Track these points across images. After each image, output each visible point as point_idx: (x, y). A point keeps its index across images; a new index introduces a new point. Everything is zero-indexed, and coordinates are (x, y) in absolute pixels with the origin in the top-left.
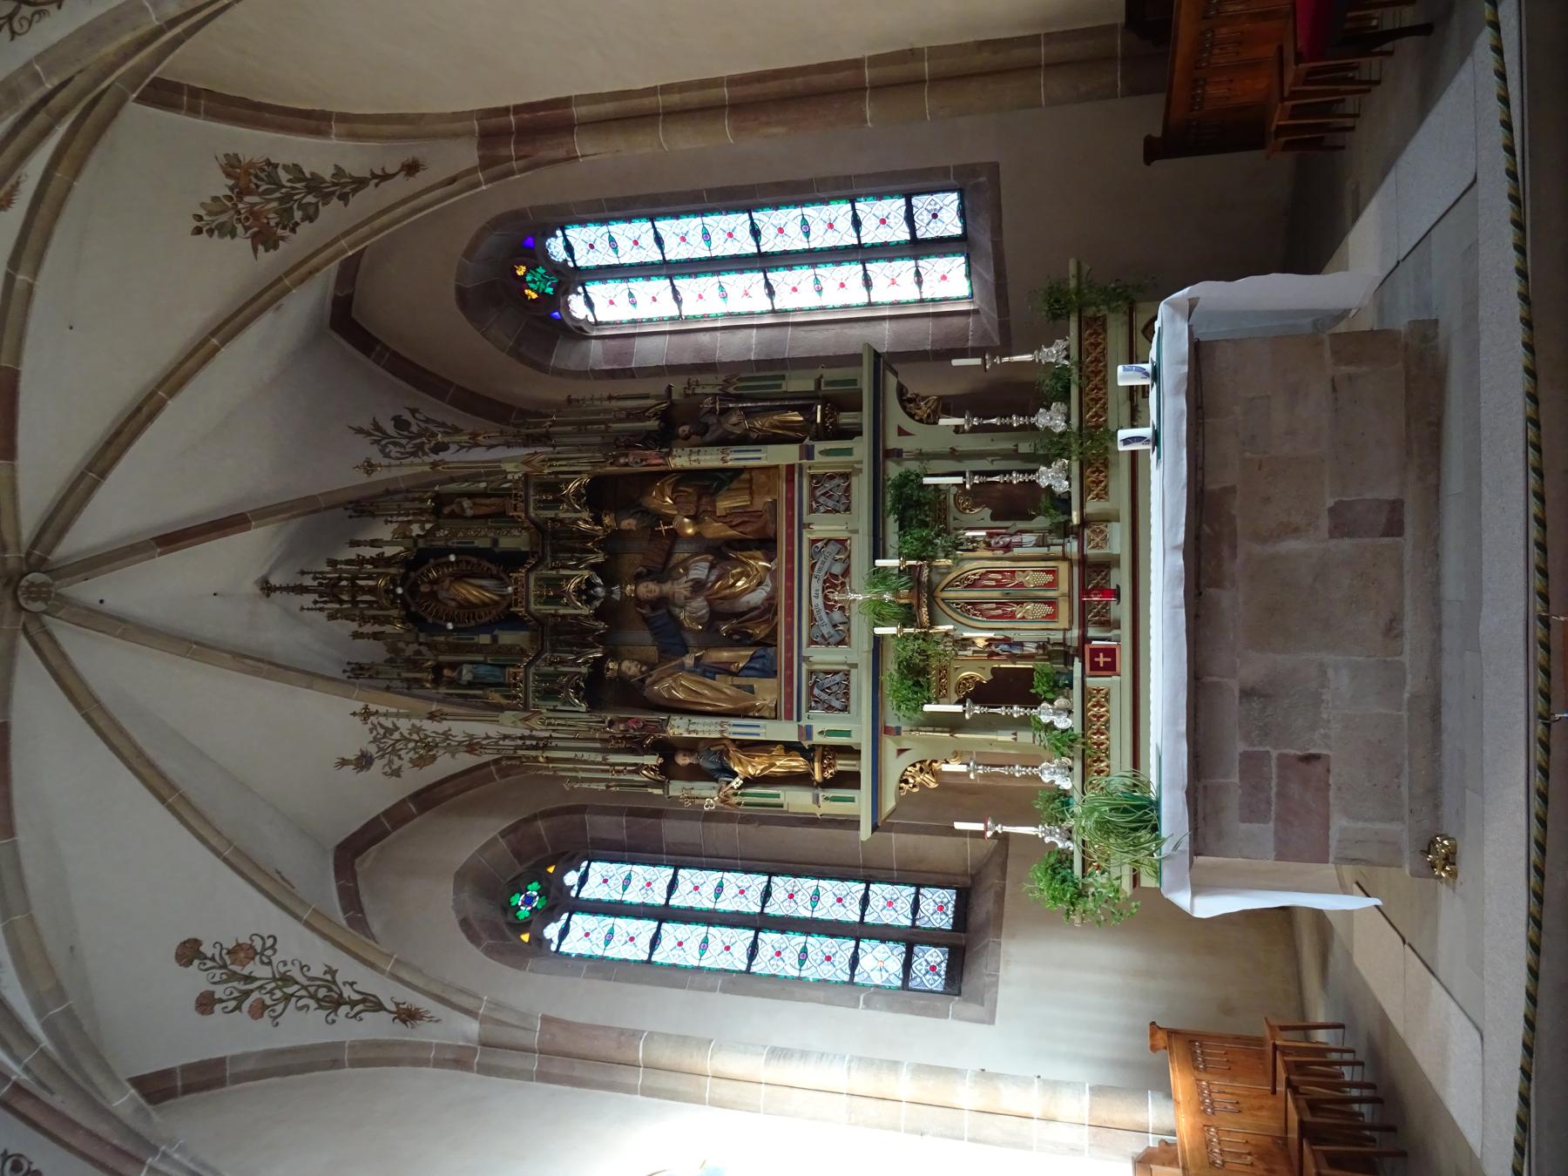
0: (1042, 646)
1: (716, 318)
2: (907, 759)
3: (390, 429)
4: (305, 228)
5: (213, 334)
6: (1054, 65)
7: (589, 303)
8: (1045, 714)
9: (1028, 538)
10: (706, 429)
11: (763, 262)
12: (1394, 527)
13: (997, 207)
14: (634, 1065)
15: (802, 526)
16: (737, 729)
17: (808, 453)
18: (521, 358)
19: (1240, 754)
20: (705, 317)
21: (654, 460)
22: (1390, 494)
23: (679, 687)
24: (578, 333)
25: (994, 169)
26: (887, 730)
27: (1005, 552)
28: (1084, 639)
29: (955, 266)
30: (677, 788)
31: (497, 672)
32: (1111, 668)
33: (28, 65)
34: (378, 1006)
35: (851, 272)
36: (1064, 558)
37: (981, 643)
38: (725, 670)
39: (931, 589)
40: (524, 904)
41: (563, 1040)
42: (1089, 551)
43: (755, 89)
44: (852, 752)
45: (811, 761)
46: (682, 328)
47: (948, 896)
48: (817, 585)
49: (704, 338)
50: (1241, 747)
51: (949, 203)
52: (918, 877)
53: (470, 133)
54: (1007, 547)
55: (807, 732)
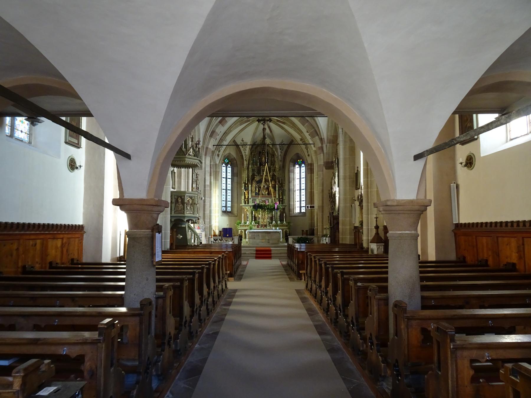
0: (259, 221)
1: (295, 183)
2: (248, 208)
5: (291, 135)
6: (312, 222)
7: (298, 168)
8: (253, 222)
9: (269, 220)
10: (280, 188)
11: (300, 190)
12: (268, 243)
16: (250, 192)
17: (277, 199)
18: (291, 160)
20: (295, 182)
21: (277, 183)
23: (254, 185)
24: (294, 166)
25: (305, 216)
26: (250, 207)
27: (277, 121)
28: (260, 225)
29: (299, 211)
30: (243, 184)
32: (257, 227)
33: (308, 140)
34: (219, 152)
35: (299, 200)
36: (267, 223)
37: (259, 216)
38: (256, 190)
39: (264, 212)
41: (217, 173)
42: (267, 225)
44: (248, 203)
46: (294, 179)
47: (230, 210)
48: (264, 200)
51: (304, 211)
52: (232, 207)
54: (268, 218)
55: (250, 199)
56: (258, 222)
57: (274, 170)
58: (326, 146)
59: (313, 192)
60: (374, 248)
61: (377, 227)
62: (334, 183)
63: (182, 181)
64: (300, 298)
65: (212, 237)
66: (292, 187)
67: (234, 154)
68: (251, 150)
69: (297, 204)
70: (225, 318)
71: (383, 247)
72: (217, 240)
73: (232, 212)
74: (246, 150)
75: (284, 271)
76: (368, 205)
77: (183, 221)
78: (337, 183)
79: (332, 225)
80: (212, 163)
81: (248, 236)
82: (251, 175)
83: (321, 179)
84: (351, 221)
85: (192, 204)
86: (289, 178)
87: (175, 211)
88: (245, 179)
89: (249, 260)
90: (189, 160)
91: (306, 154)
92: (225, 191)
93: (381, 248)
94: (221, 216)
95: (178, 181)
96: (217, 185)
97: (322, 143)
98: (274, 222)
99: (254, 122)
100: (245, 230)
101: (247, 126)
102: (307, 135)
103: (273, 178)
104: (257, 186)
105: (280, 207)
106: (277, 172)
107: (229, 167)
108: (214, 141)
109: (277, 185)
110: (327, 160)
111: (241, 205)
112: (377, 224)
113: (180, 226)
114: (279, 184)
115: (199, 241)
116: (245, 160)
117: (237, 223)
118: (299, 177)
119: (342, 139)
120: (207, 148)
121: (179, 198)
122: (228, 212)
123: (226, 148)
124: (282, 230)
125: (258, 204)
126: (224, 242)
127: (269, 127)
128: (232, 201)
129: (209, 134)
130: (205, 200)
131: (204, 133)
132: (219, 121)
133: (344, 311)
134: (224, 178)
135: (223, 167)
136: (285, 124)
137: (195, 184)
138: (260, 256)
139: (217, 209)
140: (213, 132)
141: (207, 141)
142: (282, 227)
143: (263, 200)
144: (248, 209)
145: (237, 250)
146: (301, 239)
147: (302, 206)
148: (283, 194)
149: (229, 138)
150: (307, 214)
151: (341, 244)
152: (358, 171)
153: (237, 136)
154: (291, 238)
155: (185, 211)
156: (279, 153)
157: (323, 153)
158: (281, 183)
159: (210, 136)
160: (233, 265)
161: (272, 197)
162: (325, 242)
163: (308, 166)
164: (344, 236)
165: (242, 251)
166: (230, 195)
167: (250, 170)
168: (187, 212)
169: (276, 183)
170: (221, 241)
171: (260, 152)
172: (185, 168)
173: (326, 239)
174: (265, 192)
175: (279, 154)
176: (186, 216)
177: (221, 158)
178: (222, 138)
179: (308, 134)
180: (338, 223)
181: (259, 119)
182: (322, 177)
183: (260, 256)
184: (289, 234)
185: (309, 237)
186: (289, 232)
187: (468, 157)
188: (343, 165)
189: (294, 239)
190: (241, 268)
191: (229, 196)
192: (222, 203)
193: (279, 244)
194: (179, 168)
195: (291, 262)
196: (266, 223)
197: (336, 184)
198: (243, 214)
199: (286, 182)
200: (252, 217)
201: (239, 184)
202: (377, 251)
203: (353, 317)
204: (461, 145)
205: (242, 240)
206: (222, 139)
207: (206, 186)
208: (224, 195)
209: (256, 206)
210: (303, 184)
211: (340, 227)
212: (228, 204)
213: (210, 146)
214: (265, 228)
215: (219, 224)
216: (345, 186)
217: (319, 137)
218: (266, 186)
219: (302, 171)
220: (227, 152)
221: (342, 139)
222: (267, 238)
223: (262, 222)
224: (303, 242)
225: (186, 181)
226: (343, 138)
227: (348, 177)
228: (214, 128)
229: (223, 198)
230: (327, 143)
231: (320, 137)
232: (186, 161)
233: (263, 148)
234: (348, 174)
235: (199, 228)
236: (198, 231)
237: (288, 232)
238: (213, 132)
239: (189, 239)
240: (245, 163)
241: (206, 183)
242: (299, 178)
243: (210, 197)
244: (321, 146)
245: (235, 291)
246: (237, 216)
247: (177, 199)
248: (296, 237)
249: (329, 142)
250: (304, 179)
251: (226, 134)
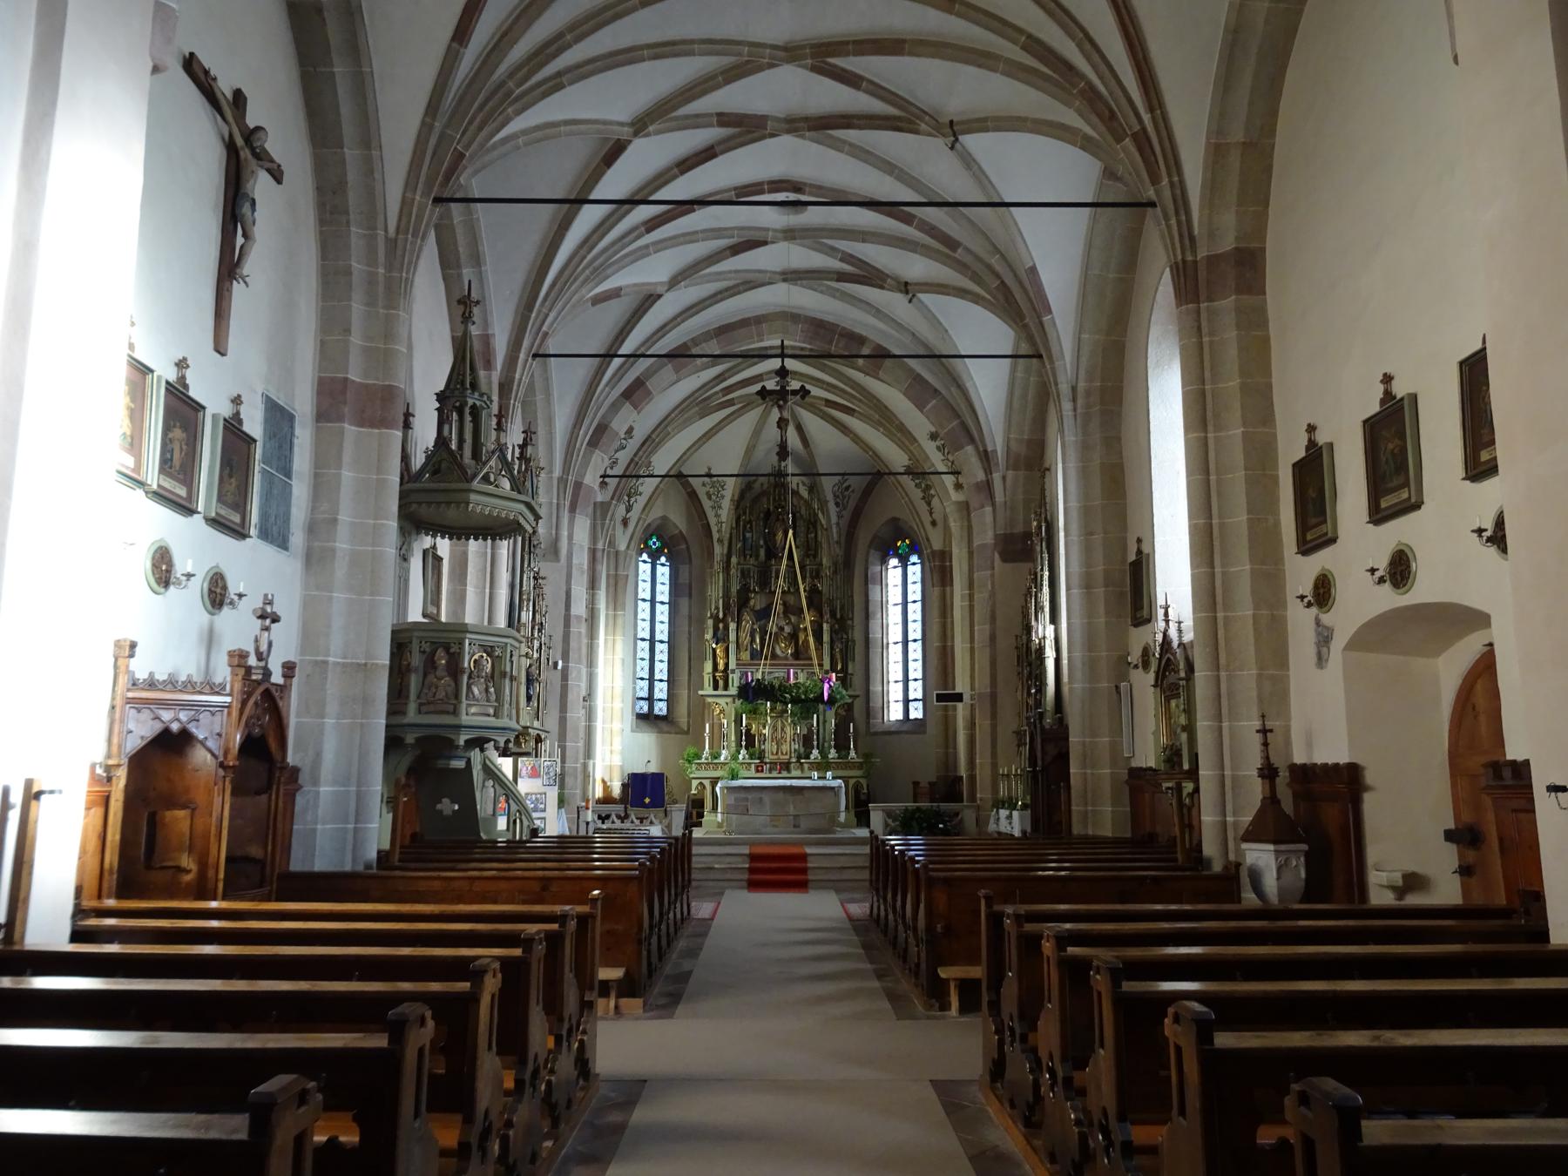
0: (764, 751)
2: (725, 706)
3: (844, 485)
4: (912, 484)
5: (874, 452)
6: (947, 754)
7: (895, 567)
8: (743, 751)
9: (797, 746)
11: (905, 642)
12: (795, 826)
15: (802, 670)
16: (732, 647)
19: (1131, 564)
20: (887, 615)
21: (827, 616)
24: (884, 561)
25: (925, 732)
28: (766, 763)
29: (900, 716)
30: (710, 622)
31: (749, 547)
32: (757, 771)
34: (628, 511)
38: (753, 640)
39: (781, 716)
40: (654, 543)
41: (620, 584)
44: (726, 687)
46: (883, 606)
47: (664, 712)
49: (879, 615)
50: (750, 797)
52: (671, 700)
55: (733, 671)
56: (760, 753)
57: (817, 575)
58: (1004, 478)
59: (949, 649)
60: (1261, 863)
61: (1268, 772)
63: (468, 592)
64: (971, 1159)
66: (875, 633)
67: (679, 520)
68: (737, 508)
69: (895, 692)
70: (630, 1124)
71: (1302, 859)
72: (608, 817)
74: (720, 507)
77: (450, 745)
78: (1047, 609)
79: (1039, 763)
80: (600, 546)
81: (723, 801)
82: (738, 592)
83: (986, 595)
84: (1115, 748)
85: (492, 677)
86: (867, 602)
88: (717, 602)
89: (722, 894)
90: (483, 502)
91: (927, 519)
92: (646, 645)
95: (452, 593)
96: (620, 621)
97: (988, 470)
98: (815, 752)
99: (750, 407)
100: (714, 781)
102: (930, 448)
104: (755, 627)
105: (839, 693)
106: (825, 579)
107: (663, 565)
108: (603, 460)
109: (825, 626)
110: (1006, 529)
111: (700, 692)
113: (441, 763)
115: (526, 823)
118: (899, 600)
119: (1073, 439)
120: (578, 485)
122: (658, 717)
125: (758, 680)
126: (632, 826)
127: (800, 429)
128: (671, 681)
131: (568, 436)
132: (623, 388)
133: (1024, 1038)
134: (644, 600)
135: (641, 564)
136: (852, 416)
137: (528, 610)
138: (766, 865)
140: (602, 429)
141: (577, 461)
142: (842, 769)
143: (777, 675)
144: (724, 706)
145: (678, 852)
146: (917, 816)
147: (910, 698)
148: (847, 655)
150: (933, 729)
152: (1139, 552)
153: (688, 458)
154: (881, 813)
155: (460, 702)
156: (832, 518)
158: (838, 616)
160: (640, 942)
161: (812, 665)
162: (1004, 827)
167: (733, 571)
169: (821, 616)
170: (623, 822)
171: (768, 514)
172: (485, 539)
173: (1010, 817)
174: (784, 649)
175: (834, 519)
176: (464, 723)
178: (636, 459)
180: (1063, 757)
183: (766, 865)
185: (944, 806)
186: (868, 786)
189: (889, 814)
191: (661, 661)
192: (638, 688)
193: (834, 832)
194: (459, 539)
197: (1043, 611)
198: (707, 725)
199: (855, 614)
201: (697, 622)
202: (1278, 878)
203: (1109, 1111)
204: (1468, 482)
205: (703, 817)
207: (573, 622)
208: (643, 659)
209: (751, 691)
212: (656, 690)
213: (591, 479)
214: (785, 774)
215: (623, 759)
216: (1090, 613)
217: (977, 448)
218: (787, 629)
220: (656, 513)
221: (1073, 439)
222: (791, 810)
223: (772, 754)
224: (925, 825)
226: (1076, 435)
229: (638, 668)
230: (1007, 469)
231: (981, 449)
235: (535, 774)
236: (525, 786)
237: (865, 786)
238: (602, 429)
240: (719, 550)
241: (572, 610)
243: (591, 663)
245: (633, 1090)
246: (687, 733)
247: (433, 653)
249: (1014, 462)
251: (652, 442)
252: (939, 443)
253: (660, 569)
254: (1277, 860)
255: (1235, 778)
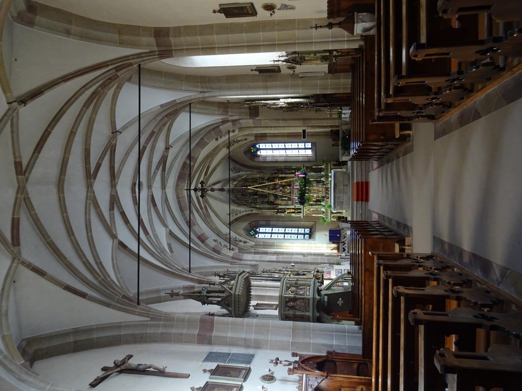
0: (322, 196)
1: (278, 155)
5: (222, 159)
6: (323, 135)
7: (260, 152)
8: (322, 203)
9: (320, 185)
10: (282, 172)
11: (286, 149)
12: (347, 186)
13: (316, 146)
14: (274, 246)
15: (295, 183)
16: (287, 207)
18: (251, 160)
21: (277, 175)
22: (347, 184)
23: (280, 202)
24: (258, 156)
28: (326, 196)
29: (310, 151)
30: (279, 214)
32: (328, 198)
34: (241, 241)
35: (297, 151)
37: (315, 196)
38: (285, 200)
39: (310, 190)
40: (252, 233)
41: (266, 244)
43: (289, 134)
44: (300, 209)
45: (295, 210)
46: (273, 157)
47: (309, 229)
49: (276, 158)
52: (304, 227)
53: (254, 136)
56: (322, 198)
57: (263, 179)
58: (231, 116)
59: (288, 134)
61: (330, 26)
62: (275, 105)
65: (341, 255)
66: (282, 159)
68: (241, 205)
69: (302, 152)
71: (360, 14)
72: (344, 248)
73: (311, 228)
74: (240, 211)
75: (390, 164)
76: (298, 43)
77: (319, 301)
78: (275, 101)
82: (268, 205)
83: (270, 122)
84: (322, 78)
87: (306, 311)
91: (244, 142)
92: (286, 235)
93: (362, 16)
94: (315, 240)
96: (278, 244)
97: (228, 121)
98: (322, 179)
100: (332, 213)
101: (213, 210)
102: (220, 141)
103: (270, 180)
104: (280, 199)
106: (264, 176)
107: (259, 230)
111: (302, 217)
112: (325, 26)
113: (326, 304)
114: (278, 173)
116: (251, 211)
117: (323, 222)
120: (233, 258)
121: (288, 305)
122: (310, 232)
123: (237, 233)
124: (331, 169)
125: (298, 198)
126: (347, 240)
128: (298, 227)
129: (216, 255)
130: (294, 262)
134: (271, 236)
135: (259, 237)
137: (274, 275)
138: (360, 196)
139: (306, 245)
140: (215, 250)
141: (225, 258)
142: (328, 170)
143: (296, 192)
144: (307, 210)
146: (344, 145)
148: (290, 169)
149: (225, 230)
150: (314, 140)
151: (351, 90)
152: (256, 70)
155: (305, 298)
156: (244, 174)
157: (239, 119)
158: (277, 171)
159: (219, 255)
160: (386, 238)
161: (293, 180)
162: (348, 116)
163: (258, 140)
164: (342, 87)
165: (358, 220)
166: (290, 229)
167: (262, 207)
168: (306, 295)
169: (277, 177)
170: (346, 244)
171: (243, 195)
172: (251, 289)
174: (288, 190)
175: (244, 173)
176: (312, 296)
177: (248, 239)
179: (219, 140)
180: (324, 96)
181: (200, 196)
182: (267, 121)
184: (336, 161)
185: (341, 136)
187: (265, 9)
188: (250, 90)
190: (384, 222)
191: (292, 230)
192: (300, 238)
194: (251, 298)
195: (375, 157)
196: (324, 188)
198: (313, 215)
200: (316, 205)
201: (279, 219)
202: (366, 22)
205: (344, 217)
206: (226, 238)
207: (278, 260)
208: (291, 237)
210: (278, 146)
211: (329, 93)
212: (301, 232)
213: (231, 254)
214: (329, 189)
215: (325, 243)
217: (221, 125)
218: (281, 188)
219: (264, 147)
220: (242, 232)
223: (323, 193)
224: (347, 142)
225: (269, 289)
226: (217, 91)
227: (264, 83)
228: (210, 250)
230: (227, 115)
231: (221, 123)
232: (239, 294)
233: (238, 191)
234: (261, 84)
235: (329, 273)
236: (333, 276)
238: (215, 250)
239: (344, 290)
242: (272, 151)
244: (231, 122)
245: (437, 240)
247: (289, 306)
248: (341, 151)
249: (226, 112)
250: (273, 144)
251: (218, 233)
252: (219, 138)
253: (261, 231)
254: (360, 23)
255: (332, 38)
